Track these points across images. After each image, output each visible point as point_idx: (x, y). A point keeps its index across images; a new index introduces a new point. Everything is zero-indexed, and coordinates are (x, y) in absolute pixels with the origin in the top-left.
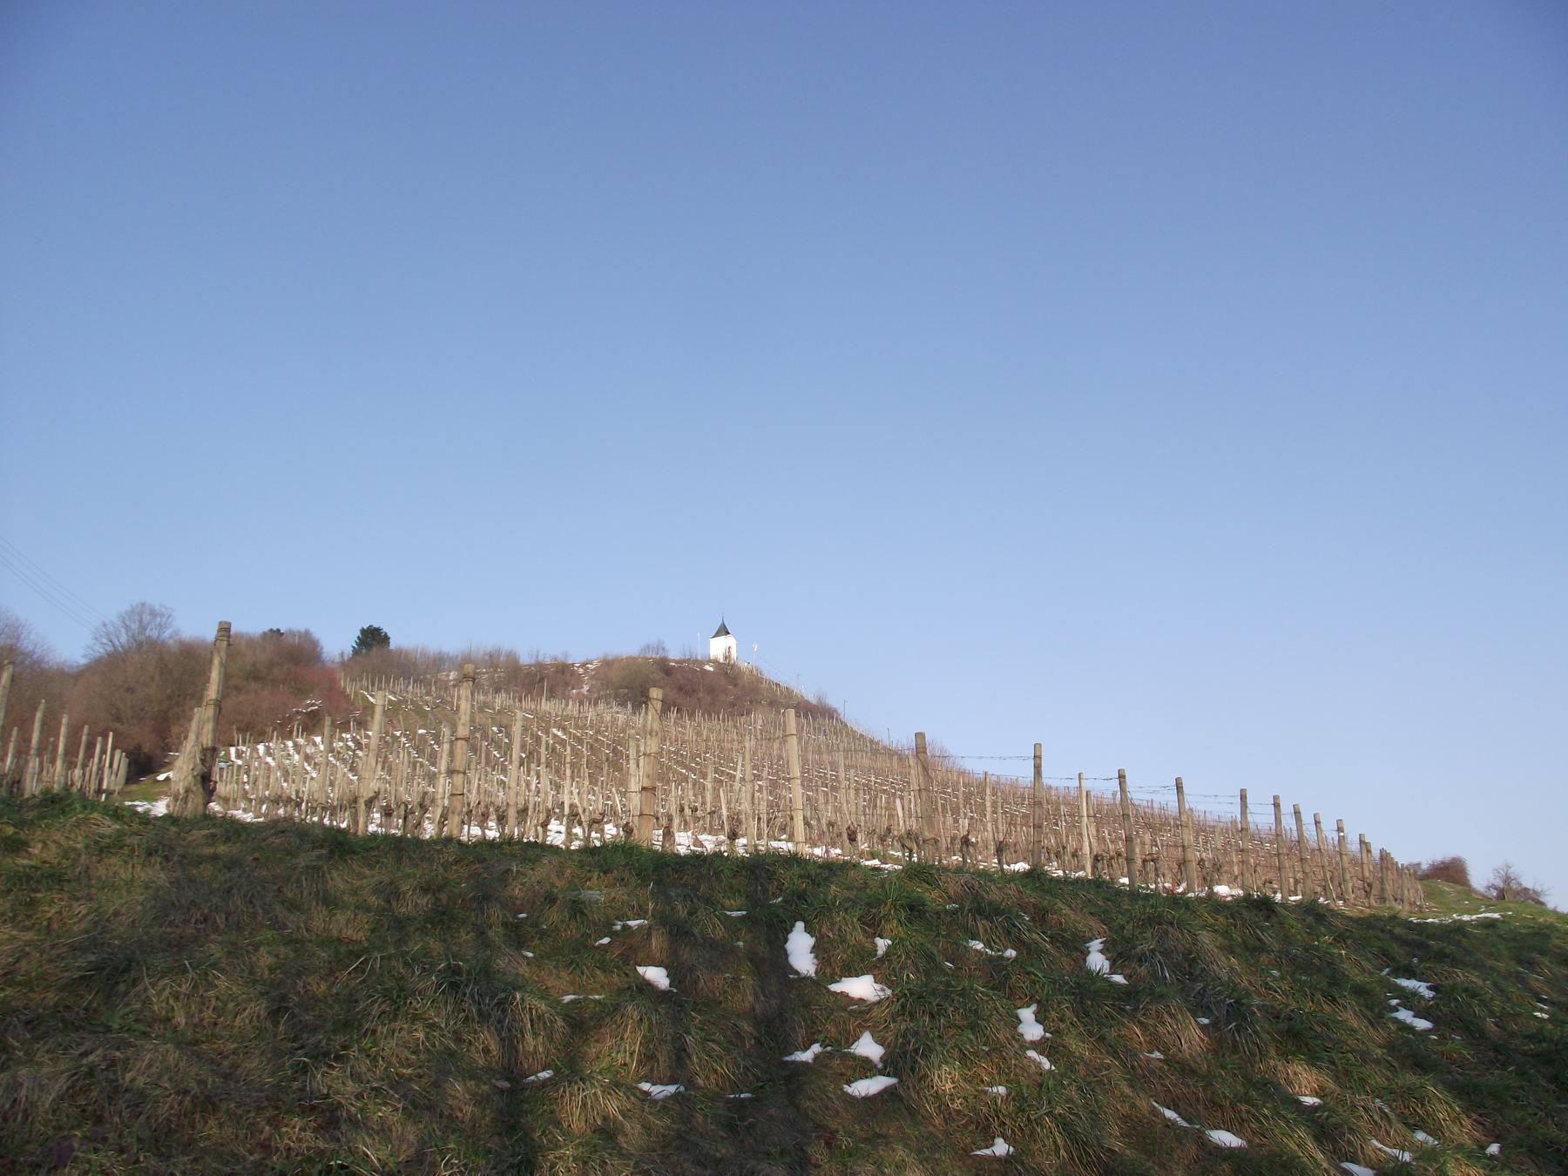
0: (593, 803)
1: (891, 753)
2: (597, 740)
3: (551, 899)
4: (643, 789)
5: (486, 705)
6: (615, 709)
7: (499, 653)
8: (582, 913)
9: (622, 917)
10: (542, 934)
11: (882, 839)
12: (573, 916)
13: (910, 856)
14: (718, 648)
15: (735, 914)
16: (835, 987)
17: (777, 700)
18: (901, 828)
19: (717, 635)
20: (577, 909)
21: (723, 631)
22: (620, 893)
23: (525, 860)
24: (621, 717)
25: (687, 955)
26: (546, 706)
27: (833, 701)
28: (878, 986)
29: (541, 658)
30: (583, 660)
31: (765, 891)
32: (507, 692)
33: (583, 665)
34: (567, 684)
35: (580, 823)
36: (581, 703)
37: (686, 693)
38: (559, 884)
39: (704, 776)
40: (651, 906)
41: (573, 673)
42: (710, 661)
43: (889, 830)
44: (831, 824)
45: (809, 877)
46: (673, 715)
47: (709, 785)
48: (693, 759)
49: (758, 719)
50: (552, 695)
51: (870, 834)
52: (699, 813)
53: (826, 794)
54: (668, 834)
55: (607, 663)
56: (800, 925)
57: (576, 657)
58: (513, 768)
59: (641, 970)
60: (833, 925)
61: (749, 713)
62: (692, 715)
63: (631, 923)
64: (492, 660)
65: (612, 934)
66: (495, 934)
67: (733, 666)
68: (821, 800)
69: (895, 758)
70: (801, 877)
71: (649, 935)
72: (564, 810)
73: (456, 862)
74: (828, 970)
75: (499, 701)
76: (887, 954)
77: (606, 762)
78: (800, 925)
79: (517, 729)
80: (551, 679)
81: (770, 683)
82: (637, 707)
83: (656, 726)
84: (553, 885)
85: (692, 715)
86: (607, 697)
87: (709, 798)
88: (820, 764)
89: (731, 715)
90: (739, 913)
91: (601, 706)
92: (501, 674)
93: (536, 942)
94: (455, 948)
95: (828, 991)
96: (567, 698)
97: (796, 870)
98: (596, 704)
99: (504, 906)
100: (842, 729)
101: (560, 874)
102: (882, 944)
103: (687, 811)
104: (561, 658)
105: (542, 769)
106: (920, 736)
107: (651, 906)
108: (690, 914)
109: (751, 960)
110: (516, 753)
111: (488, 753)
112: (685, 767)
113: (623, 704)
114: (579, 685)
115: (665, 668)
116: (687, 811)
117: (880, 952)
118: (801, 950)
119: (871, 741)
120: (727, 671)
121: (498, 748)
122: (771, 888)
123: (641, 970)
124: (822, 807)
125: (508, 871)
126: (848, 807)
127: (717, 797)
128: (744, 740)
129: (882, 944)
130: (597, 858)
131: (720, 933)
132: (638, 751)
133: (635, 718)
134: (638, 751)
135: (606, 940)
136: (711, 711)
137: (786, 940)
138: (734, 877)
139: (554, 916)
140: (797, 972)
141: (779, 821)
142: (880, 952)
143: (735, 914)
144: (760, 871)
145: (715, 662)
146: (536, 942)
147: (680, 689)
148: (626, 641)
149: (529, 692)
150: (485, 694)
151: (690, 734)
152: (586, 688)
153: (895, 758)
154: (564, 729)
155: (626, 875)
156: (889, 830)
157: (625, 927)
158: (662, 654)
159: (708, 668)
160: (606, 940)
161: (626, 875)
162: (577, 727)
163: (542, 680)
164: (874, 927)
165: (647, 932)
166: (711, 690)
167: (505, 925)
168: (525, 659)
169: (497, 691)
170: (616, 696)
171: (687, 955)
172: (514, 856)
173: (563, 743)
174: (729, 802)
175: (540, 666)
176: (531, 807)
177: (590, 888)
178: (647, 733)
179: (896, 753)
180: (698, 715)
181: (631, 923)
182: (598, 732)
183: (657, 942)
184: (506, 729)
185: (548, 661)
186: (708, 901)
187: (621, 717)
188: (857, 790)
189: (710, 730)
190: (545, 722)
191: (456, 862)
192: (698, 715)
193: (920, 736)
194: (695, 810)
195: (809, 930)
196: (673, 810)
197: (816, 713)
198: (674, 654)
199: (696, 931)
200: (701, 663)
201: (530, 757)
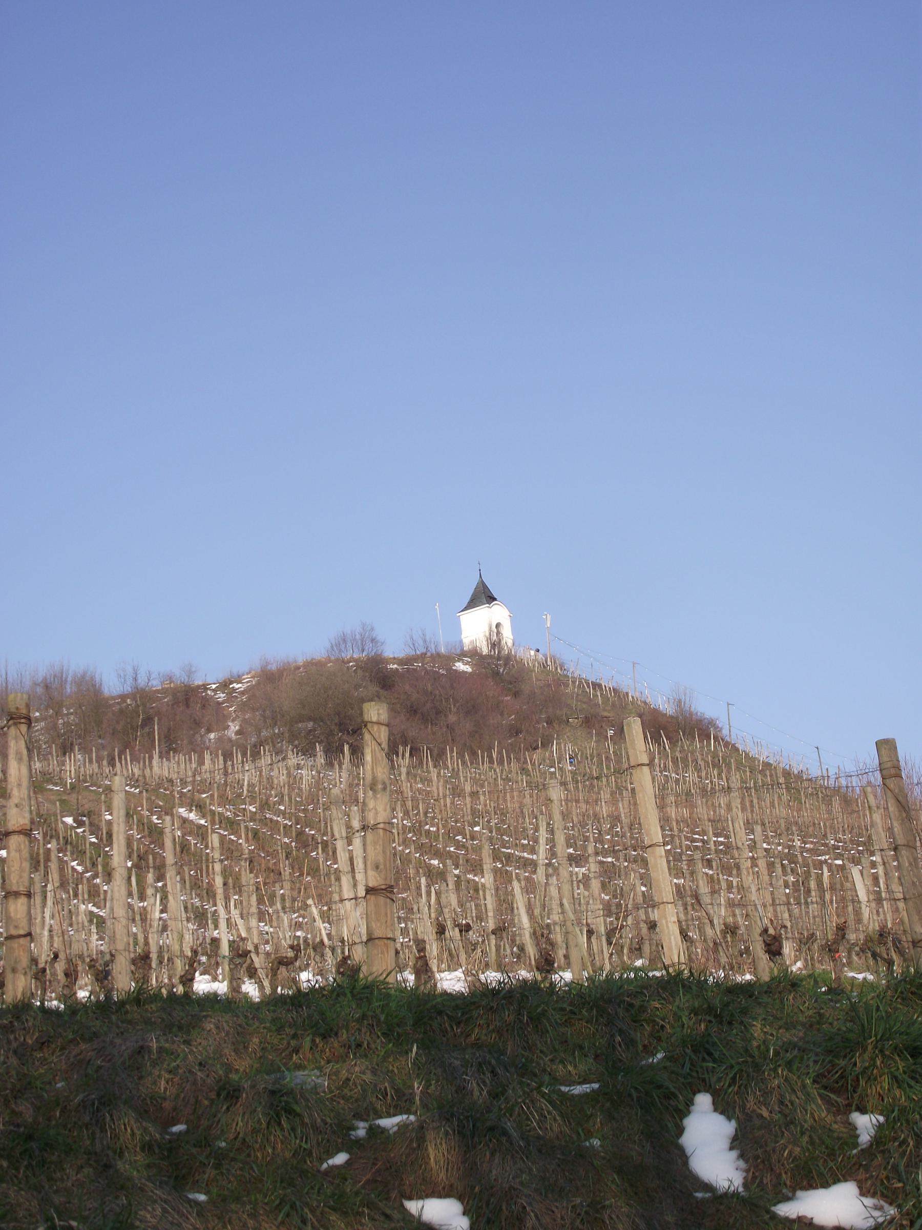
0: (284, 932)
1: (828, 793)
2: (264, 821)
3: (229, 1093)
4: (370, 891)
5: (47, 777)
6: (293, 760)
7: (60, 677)
8: (290, 1111)
9: (368, 1113)
10: (220, 1158)
11: (831, 949)
12: (275, 1120)
13: (890, 970)
14: (476, 627)
15: (578, 1090)
16: (788, 1210)
17: (600, 714)
18: (871, 919)
19: (473, 603)
20: (281, 1104)
21: (483, 596)
22: (358, 1070)
23: (169, 1028)
24: (306, 775)
25: (500, 1171)
26: (161, 768)
27: (705, 706)
28: (869, 1201)
29: (142, 681)
30: (222, 676)
31: (631, 1043)
32: (85, 750)
33: (224, 686)
34: (197, 724)
35: (252, 973)
36: (228, 756)
37: (425, 719)
38: (242, 1065)
39: (477, 868)
40: (417, 1087)
41: (206, 702)
42: (462, 655)
43: (841, 930)
44: (731, 930)
45: (710, 1010)
46: (404, 762)
47: (487, 880)
48: (449, 837)
49: (564, 747)
50: (170, 747)
51: (805, 942)
52: (472, 936)
53: (711, 879)
54: (423, 969)
55: (269, 678)
56: (703, 1101)
57: (208, 673)
58: (116, 889)
59: (413, 1206)
60: (766, 1093)
61: (546, 744)
62: (439, 758)
63: (389, 1123)
64: (50, 693)
65: (351, 1146)
66: (133, 1166)
67: (508, 658)
68: (704, 889)
69: (836, 803)
70: (695, 1011)
71: (421, 1139)
72: (222, 940)
73: (42, 1044)
74: (767, 1179)
75: (73, 766)
76: (879, 1140)
77: (293, 856)
78: (703, 1101)
79: (114, 817)
80: (167, 717)
81: (582, 683)
82: (333, 752)
83: (382, 772)
84: (229, 1068)
85: (439, 758)
86: (273, 740)
87: (490, 902)
88: (692, 823)
89: (512, 749)
90: (586, 1088)
91: (265, 761)
92: (69, 717)
93: (210, 1172)
94: (57, 1199)
95: (774, 1216)
96: (198, 750)
97: (682, 1000)
98: (256, 755)
99: (143, 1113)
100: (730, 757)
101: (240, 1047)
102: (865, 1124)
103: (453, 933)
104: (180, 676)
105: (172, 878)
106: (886, 747)
107: (417, 1087)
108: (494, 1096)
109: (619, 1171)
110: (118, 855)
111: (62, 864)
112: (437, 854)
113: (307, 751)
114: (221, 722)
115: (380, 676)
116: (453, 933)
117: (865, 1138)
118: (710, 1146)
119: (787, 774)
120: (497, 668)
121: (79, 854)
122: (642, 1036)
123: (413, 1206)
124: (706, 899)
125: (141, 1050)
126: (762, 896)
127: (506, 904)
128: (548, 791)
129: (865, 1124)
130: (303, 1017)
131: (555, 1126)
132: (349, 827)
133: (333, 774)
134: (349, 827)
135: (340, 1159)
136: (474, 746)
137: (681, 1130)
138: (568, 1023)
139: (239, 1122)
140: (708, 1187)
141: (628, 934)
142: (865, 1138)
143: (578, 1090)
144: (614, 1008)
145: (474, 654)
146: (210, 1172)
147: (413, 711)
148: (300, 632)
149: (126, 745)
150: (44, 758)
151: (437, 787)
152: (234, 727)
153: (836, 803)
154: (200, 808)
155: (366, 1038)
156: (841, 930)
157: (375, 1132)
158: (370, 650)
159: (461, 666)
160: (340, 1159)
161: (366, 1038)
162: (224, 800)
163: (148, 721)
164: (848, 1094)
165: (416, 1137)
166: (471, 709)
167: (147, 1147)
168: (112, 685)
169: (66, 749)
170: (293, 737)
171: (500, 1171)
172: (148, 1022)
173: (201, 833)
174: (530, 909)
175: (143, 696)
176: (154, 956)
177: (299, 1067)
178: (365, 805)
179: (837, 790)
180: (452, 757)
181: (389, 1123)
182: (265, 805)
183: (438, 1153)
184: (88, 817)
185: (156, 684)
186: (524, 1071)
187: (306, 775)
188: (771, 866)
189: (475, 781)
190: (162, 796)
191: (42, 1044)
192: (452, 757)
193: (886, 747)
194: (465, 929)
195: (722, 1107)
196: (427, 931)
197: (678, 731)
198: (394, 647)
199: (509, 1125)
200: (447, 660)
201: (144, 861)
